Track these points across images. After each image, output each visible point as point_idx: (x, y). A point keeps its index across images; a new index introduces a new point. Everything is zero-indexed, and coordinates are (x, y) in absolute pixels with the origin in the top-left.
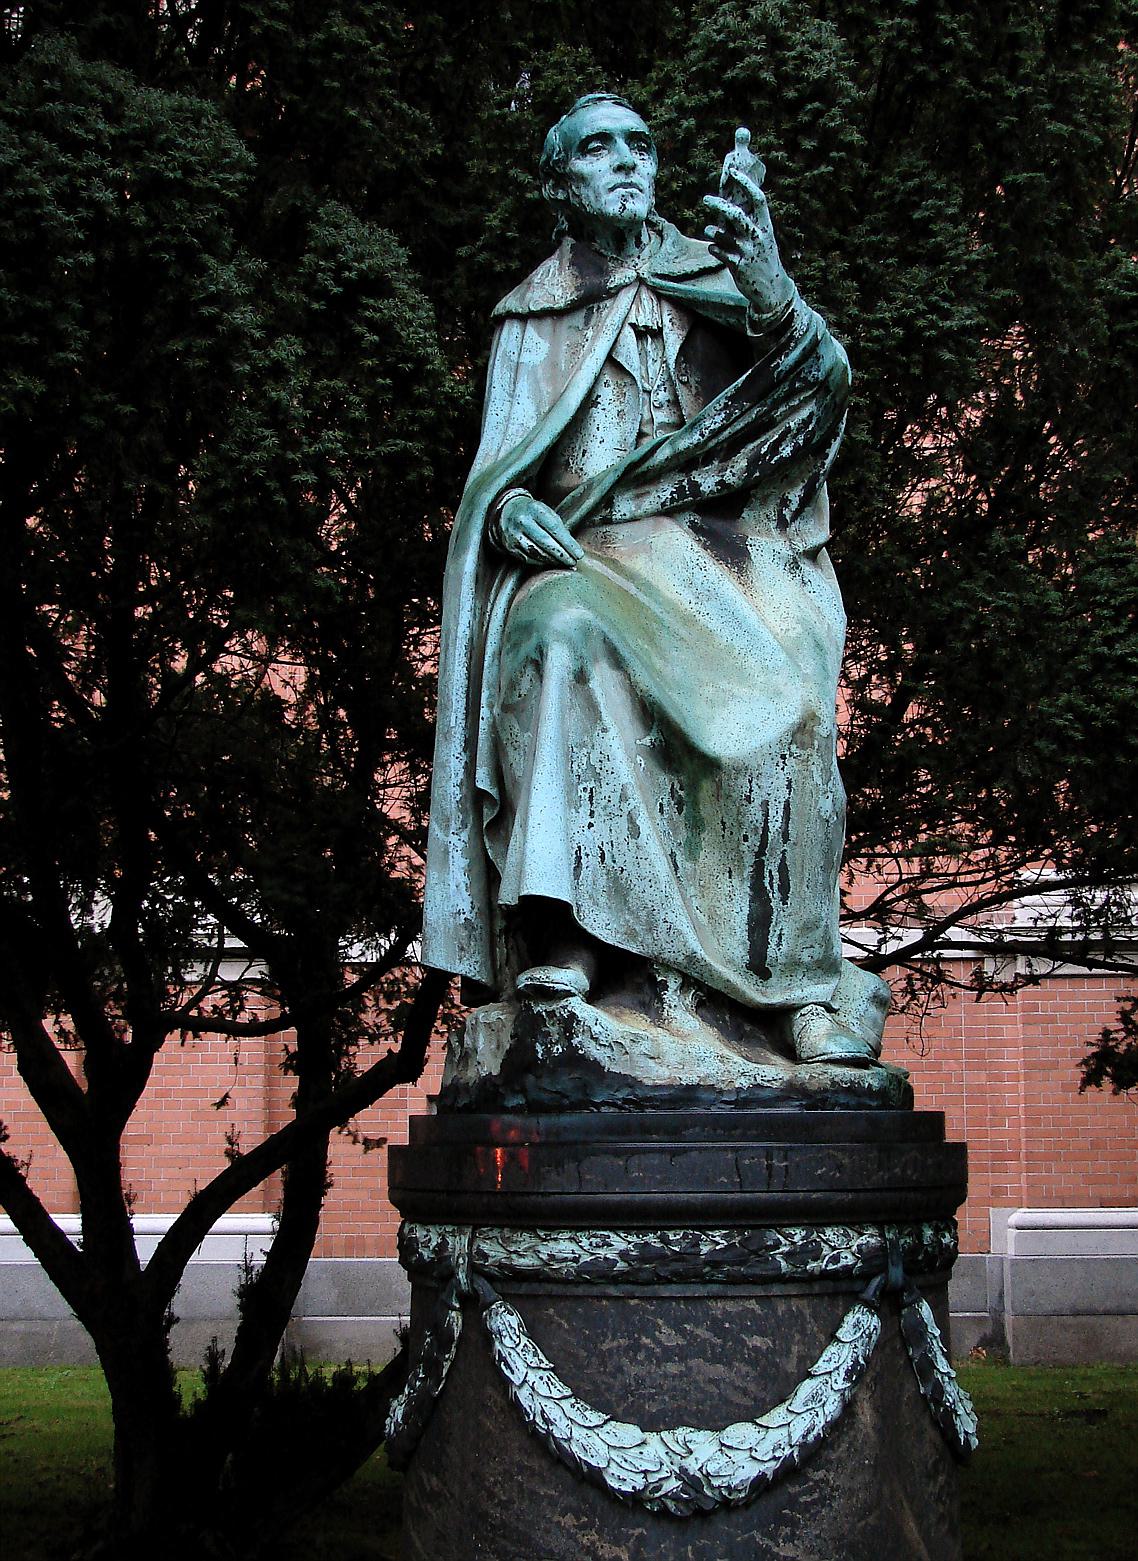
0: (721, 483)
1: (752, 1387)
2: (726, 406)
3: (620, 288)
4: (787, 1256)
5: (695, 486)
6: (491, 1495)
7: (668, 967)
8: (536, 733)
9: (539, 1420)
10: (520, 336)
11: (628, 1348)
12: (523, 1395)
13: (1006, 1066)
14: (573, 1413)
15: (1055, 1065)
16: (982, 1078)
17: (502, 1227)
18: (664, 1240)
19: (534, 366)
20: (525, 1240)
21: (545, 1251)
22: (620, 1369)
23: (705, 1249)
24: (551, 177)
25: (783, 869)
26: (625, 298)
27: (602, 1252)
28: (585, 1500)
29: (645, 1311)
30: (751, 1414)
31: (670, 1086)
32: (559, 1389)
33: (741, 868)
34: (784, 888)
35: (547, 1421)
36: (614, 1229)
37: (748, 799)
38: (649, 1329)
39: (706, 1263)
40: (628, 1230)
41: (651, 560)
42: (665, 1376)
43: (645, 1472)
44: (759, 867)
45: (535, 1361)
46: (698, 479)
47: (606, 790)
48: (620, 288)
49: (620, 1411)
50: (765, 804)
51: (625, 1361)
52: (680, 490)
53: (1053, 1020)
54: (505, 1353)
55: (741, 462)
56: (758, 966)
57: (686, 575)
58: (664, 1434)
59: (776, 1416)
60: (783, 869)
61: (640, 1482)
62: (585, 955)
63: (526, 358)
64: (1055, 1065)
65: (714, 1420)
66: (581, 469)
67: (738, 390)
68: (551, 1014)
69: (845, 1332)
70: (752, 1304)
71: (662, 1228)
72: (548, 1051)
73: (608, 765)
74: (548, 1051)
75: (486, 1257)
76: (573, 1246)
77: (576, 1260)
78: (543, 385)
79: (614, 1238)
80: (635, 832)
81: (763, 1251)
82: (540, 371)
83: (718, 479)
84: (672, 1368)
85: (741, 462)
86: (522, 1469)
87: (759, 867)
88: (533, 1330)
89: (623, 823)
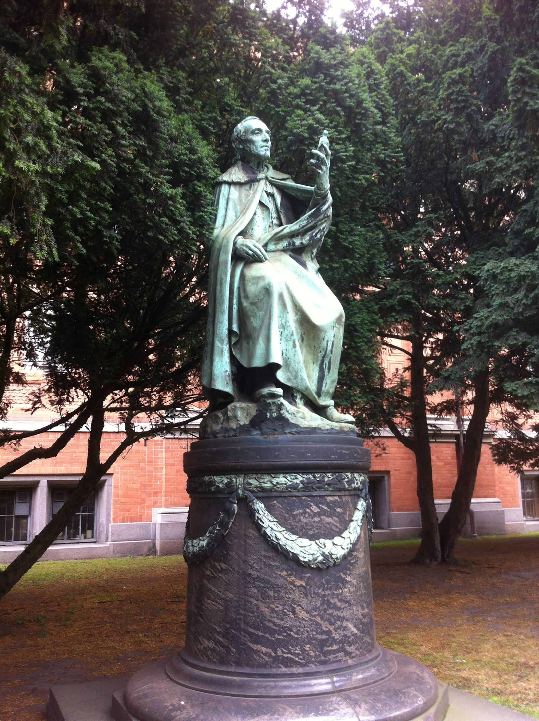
0: (302, 243)
1: (338, 525)
3: (261, 179)
4: (347, 482)
5: (294, 243)
6: (252, 567)
7: (298, 391)
9: (274, 539)
11: (303, 513)
12: (268, 531)
13: (160, 465)
14: (286, 536)
15: (174, 465)
16: (152, 468)
17: (257, 474)
18: (315, 477)
20: (267, 478)
21: (274, 481)
22: (300, 520)
23: (326, 479)
25: (330, 362)
26: (263, 182)
27: (295, 481)
28: (289, 566)
29: (308, 501)
30: (339, 534)
31: (309, 428)
32: (281, 529)
33: (317, 361)
34: (329, 369)
35: (278, 539)
36: (298, 473)
37: (324, 339)
38: (309, 507)
39: (327, 484)
40: (303, 473)
42: (314, 522)
43: (313, 554)
44: (323, 361)
45: (271, 519)
46: (295, 241)
47: (286, 332)
48: (261, 179)
49: (300, 534)
50: (328, 341)
51: (302, 518)
52: (289, 244)
53: (174, 451)
54: (260, 517)
55: (307, 238)
56: (319, 394)
58: (317, 541)
59: (345, 534)
60: (330, 362)
61: (311, 558)
62: (410, 364)
63: (231, 196)
64: (174, 465)
65: (330, 536)
67: (312, 214)
68: (274, 403)
69: (359, 507)
70: (337, 498)
71: (313, 473)
72: (271, 415)
73: (288, 324)
74: (271, 415)
75: (251, 484)
76: (285, 479)
77: (286, 484)
79: (298, 476)
80: (294, 346)
81: (340, 481)
84: (316, 519)
85: (307, 238)
86: (265, 557)
87: (323, 361)
88: (269, 508)
89: (291, 343)
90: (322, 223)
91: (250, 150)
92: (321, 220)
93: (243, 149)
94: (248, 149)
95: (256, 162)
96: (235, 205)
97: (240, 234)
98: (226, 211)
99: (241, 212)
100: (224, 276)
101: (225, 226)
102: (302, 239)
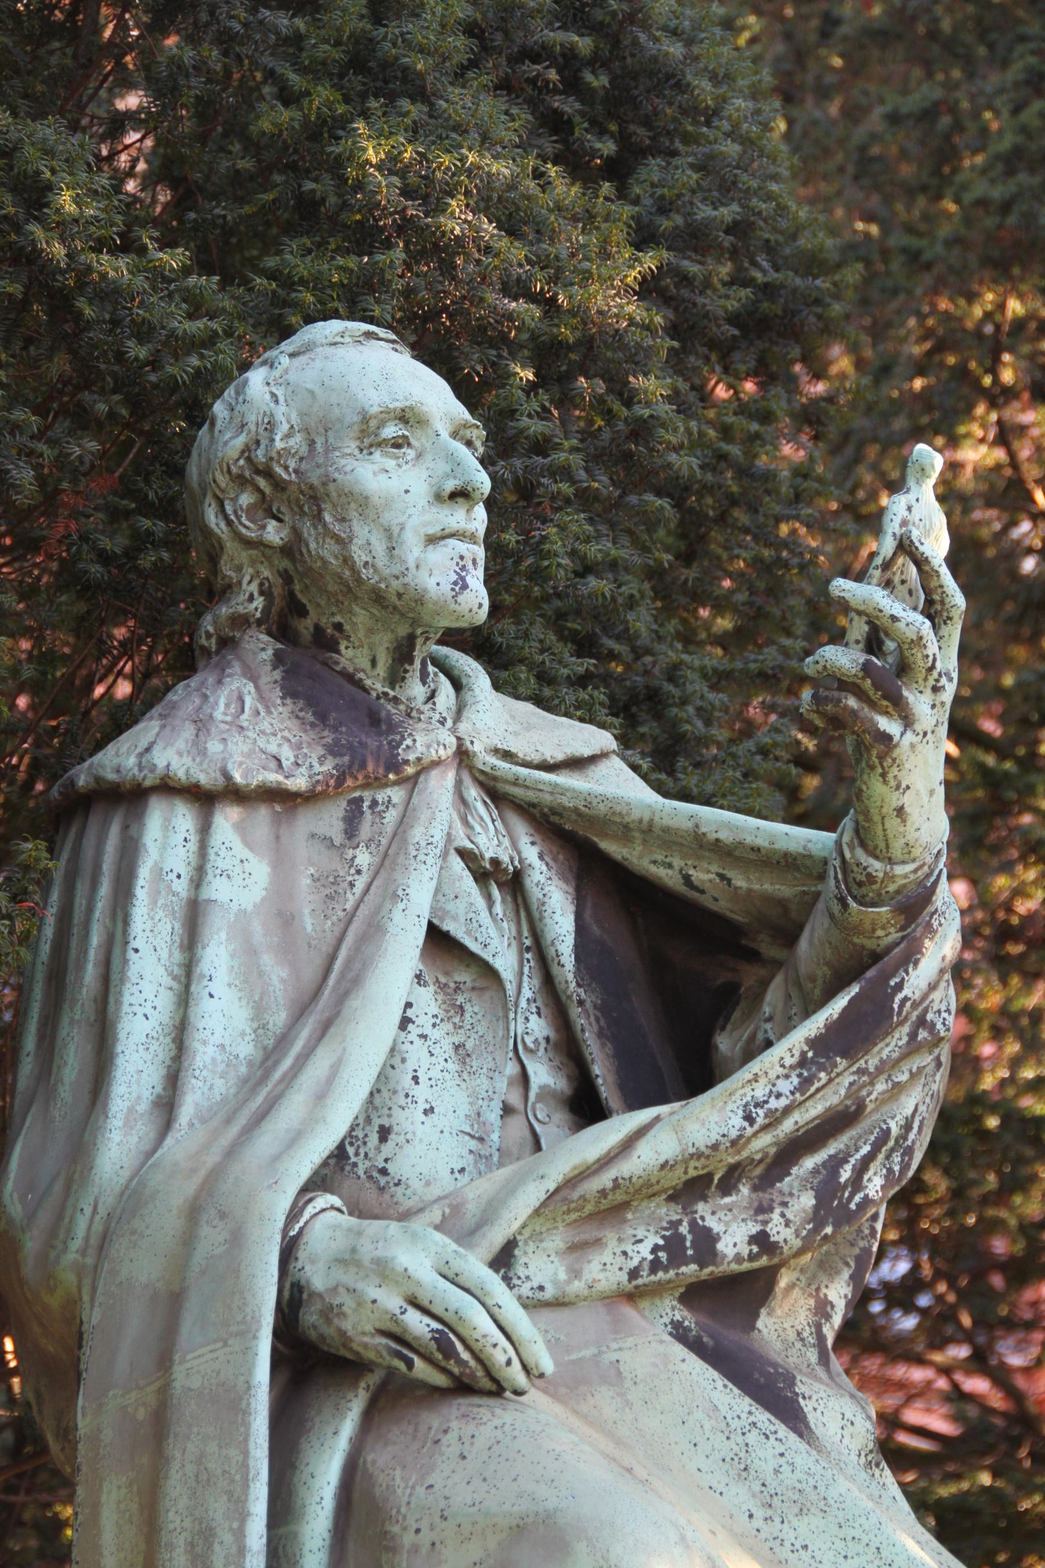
2: (803, 1062)
5: (706, 1240)
8: (929, 1530)
10: (194, 839)
19: (242, 913)
24: (663, 599)
41: (629, 1404)
46: (711, 1223)
48: (426, 767)
52: (673, 1246)
57: (726, 1449)
63: (217, 889)
66: (384, 1172)
67: (832, 1027)
78: (267, 960)
82: (257, 929)
83: (754, 1229)
90: (897, 1090)
91: (347, 560)
92: (885, 1068)
93: (291, 550)
94: (328, 551)
95: (383, 645)
96: (248, 952)
97: (317, 1183)
98: (184, 999)
99: (300, 1011)
100: (218, 1508)
101: (186, 1112)
102: (762, 1209)
